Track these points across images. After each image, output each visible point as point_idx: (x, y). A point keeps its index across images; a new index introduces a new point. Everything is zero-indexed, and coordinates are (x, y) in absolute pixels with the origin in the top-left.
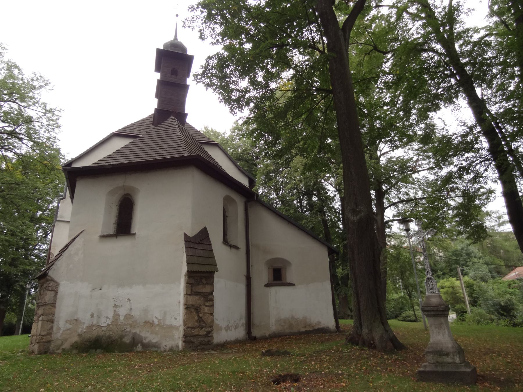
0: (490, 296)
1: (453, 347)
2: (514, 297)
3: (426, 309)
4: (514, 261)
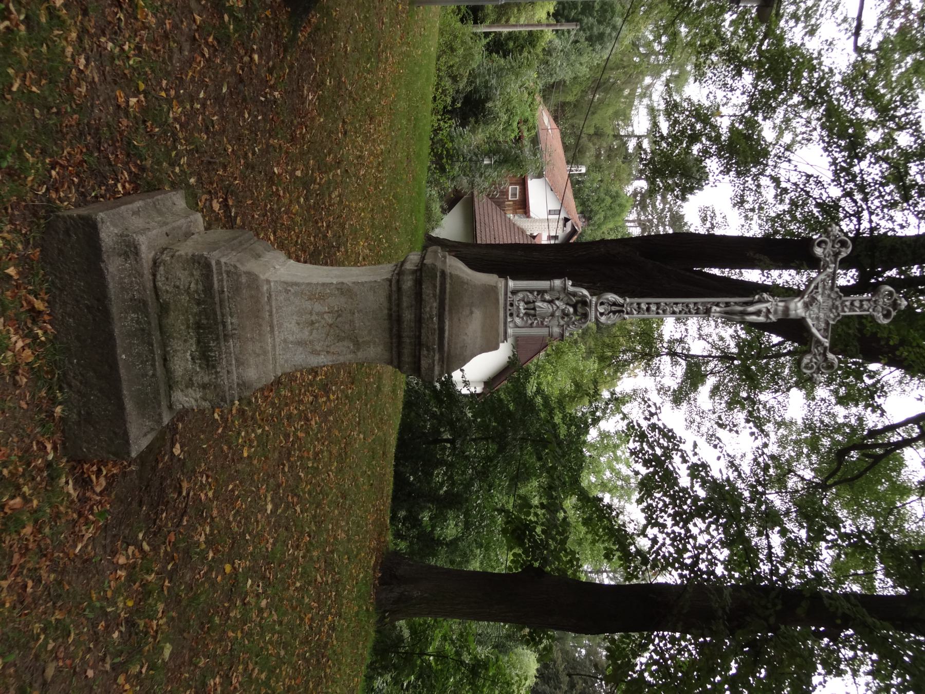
1: (243, 385)
3: (427, 290)
4: (572, 117)
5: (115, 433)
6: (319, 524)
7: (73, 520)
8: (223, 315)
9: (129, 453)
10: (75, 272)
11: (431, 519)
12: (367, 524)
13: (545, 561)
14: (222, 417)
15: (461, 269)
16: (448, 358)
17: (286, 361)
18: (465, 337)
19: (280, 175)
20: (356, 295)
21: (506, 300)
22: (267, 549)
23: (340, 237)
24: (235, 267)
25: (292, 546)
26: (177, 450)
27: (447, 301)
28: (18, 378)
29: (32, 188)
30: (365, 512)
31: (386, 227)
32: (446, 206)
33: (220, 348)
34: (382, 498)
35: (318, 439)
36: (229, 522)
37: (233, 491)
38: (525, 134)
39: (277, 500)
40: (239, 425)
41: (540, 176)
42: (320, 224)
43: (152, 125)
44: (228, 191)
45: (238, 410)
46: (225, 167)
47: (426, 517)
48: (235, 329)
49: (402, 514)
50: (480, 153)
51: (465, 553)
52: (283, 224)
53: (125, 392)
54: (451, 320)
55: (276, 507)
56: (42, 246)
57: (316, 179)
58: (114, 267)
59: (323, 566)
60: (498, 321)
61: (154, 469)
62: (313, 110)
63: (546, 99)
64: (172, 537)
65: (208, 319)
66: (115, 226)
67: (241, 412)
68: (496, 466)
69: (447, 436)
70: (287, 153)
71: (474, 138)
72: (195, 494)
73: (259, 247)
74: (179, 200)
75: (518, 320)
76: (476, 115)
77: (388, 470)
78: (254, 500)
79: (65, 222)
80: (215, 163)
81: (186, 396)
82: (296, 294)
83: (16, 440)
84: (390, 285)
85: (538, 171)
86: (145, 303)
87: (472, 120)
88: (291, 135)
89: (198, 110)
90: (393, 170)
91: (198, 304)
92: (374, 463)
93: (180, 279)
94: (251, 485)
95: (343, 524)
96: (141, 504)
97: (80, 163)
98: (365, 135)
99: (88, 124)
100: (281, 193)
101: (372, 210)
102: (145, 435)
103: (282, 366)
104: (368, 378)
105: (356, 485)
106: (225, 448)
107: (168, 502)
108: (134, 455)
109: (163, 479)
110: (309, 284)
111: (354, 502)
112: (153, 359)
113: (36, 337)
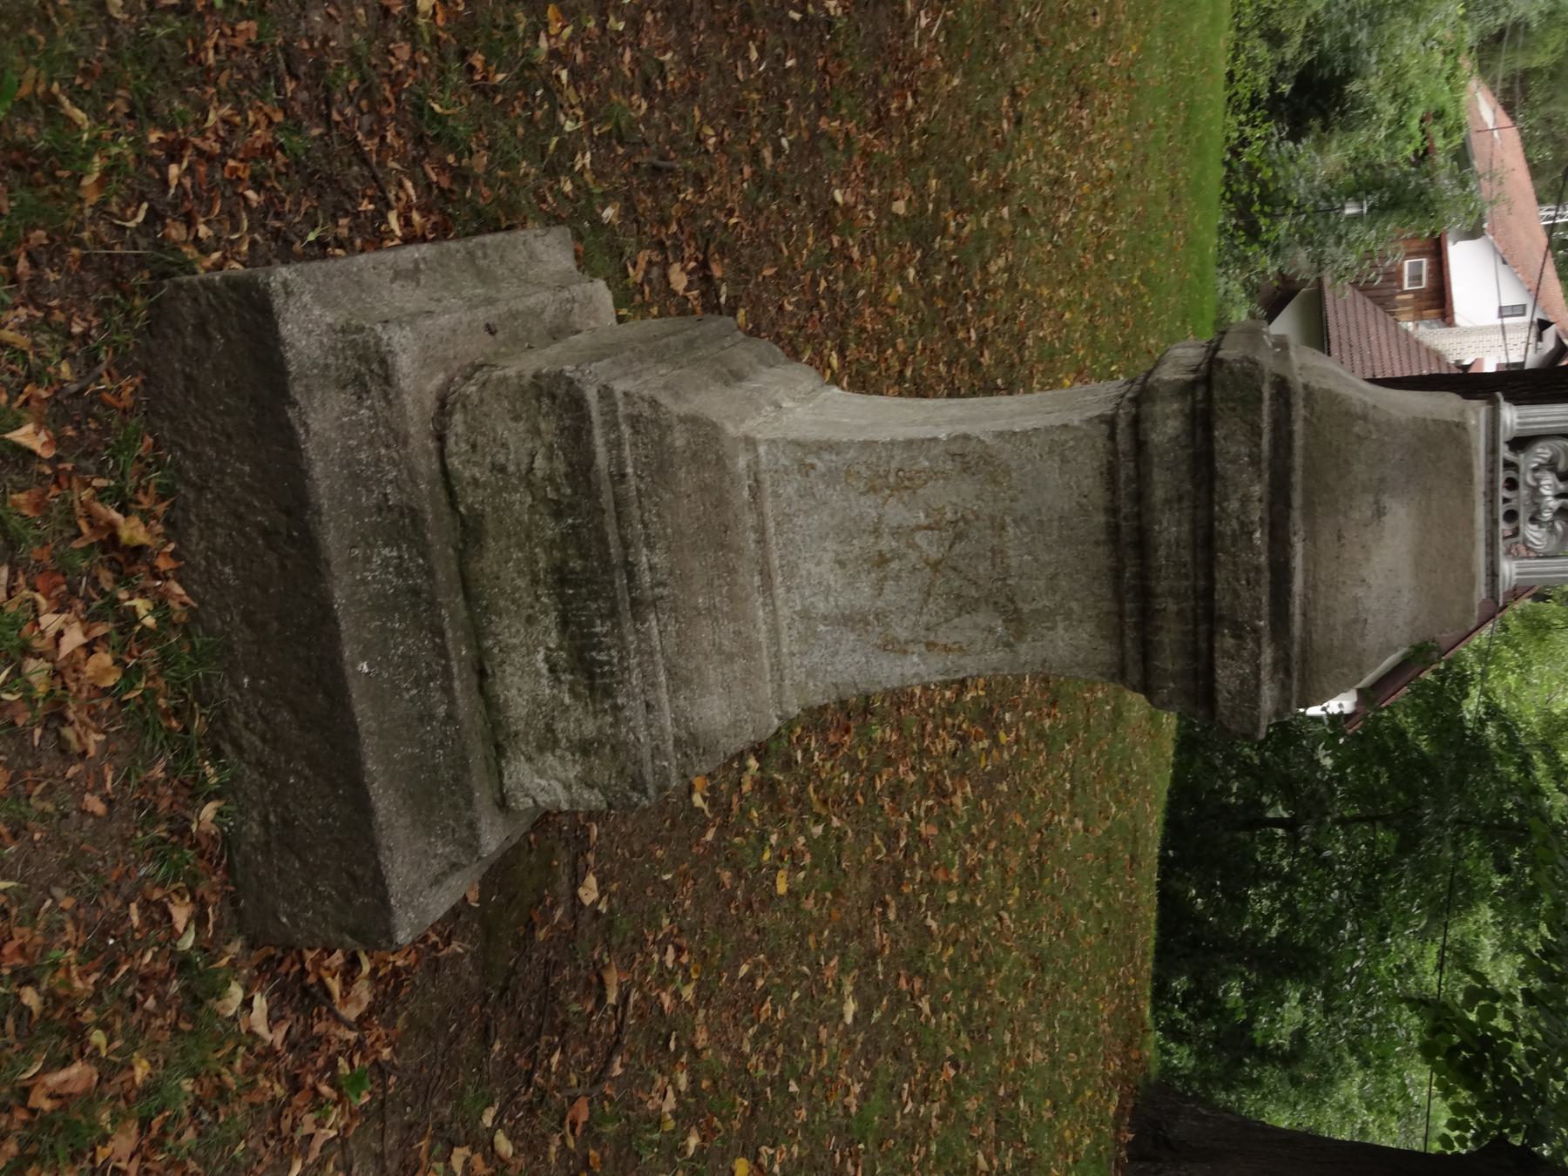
0: (1393, 36)
1: (691, 743)
2: (1383, 133)
3: (1230, 443)
4: (1546, 101)
5: (353, 878)
6: (978, 1036)
7: (273, 1101)
8: (626, 545)
9: (389, 934)
10: (229, 437)
11: (1246, 995)
12: (1096, 1023)
13: (1538, 1133)
14: (713, 801)
15: (1338, 376)
16: (1304, 660)
17: (811, 673)
18: (1360, 592)
19: (847, 209)
20: (1007, 472)
21: (1492, 471)
22: (846, 1108)
23: (1012, 366)
24: (654, 403)
25: (911, 1094)
26: (589, 892)
27: (1297, 478)
28: (68, 733)
29: (101, 206)
30: (1093, 994)
31: (1125, 347)
32: (1261, 312)
33: (622, 638)
34: (1131, 959)
35: (972, 839)
36: (739, 1055)
37: (751, 978)
38: (1439, 143)
39: (870, 991)
40: (762, 818)
41: (1474, 233)
42: (961, 335)
43: (486, 63)
44: (709, 244)
45: (759, 784)
46: (700, 183)
47: (1234, 992)
48: (663, 584)
49: (1180, 984)
50: (1331, 196)
51: (1325, 1064)
52: (863, 330)
53: (370, 765)
54: (1311, 537)
55: (866, 1007)
56: (147, 371)
57: (947, 225)
58: (323, 418)
59: (992, 1131)
60: (1471, 535)
61: (524, 943)
62: (931, 54)
63: (1484, 70)
64: (582, 1112)
65: (584, 556)
66: (330, 304)
67: (766, 787)
68: (1397, 881)
69: (1281, 812)
70: (866, 154)
71: (1322, 161)
72: (644, 997)
73: (744, 353)
74: (550, 251)
75: (1532, 533)
76: (1324, 114)
77: (1145, 896)
78: (807, 995)
79: (195, 300)
80: (671, 170)
81: (541, 773)
82: (831, 477)
83: (67, 903)
84: (1112, 437)
85: (1472, 220)
86: (415, 515)
87: (1315, 124)
88: (877, 111)
89: (620, 34)
90: (1139, 219)
91: (558, 515)
92: (1110, 882)
93: (504, 445)
94: (799, 960)
95: (1039, 1027)
96: (485, 1038)
97: (268, 151)
98: (1069, 133)
99: (287, 48)
100: (855, 253)
101: (1091, 308)
102: (437, 881)
103: (799, 687)
104: (1091, 690)
105: (1070, 937)
106: (726, 876)
107: (565, 1024)
108: (403, 936)
109: (551, 967)
110: (867, 445)
111: (1064, 975)
112: (447, 673)
113: (132, 616)
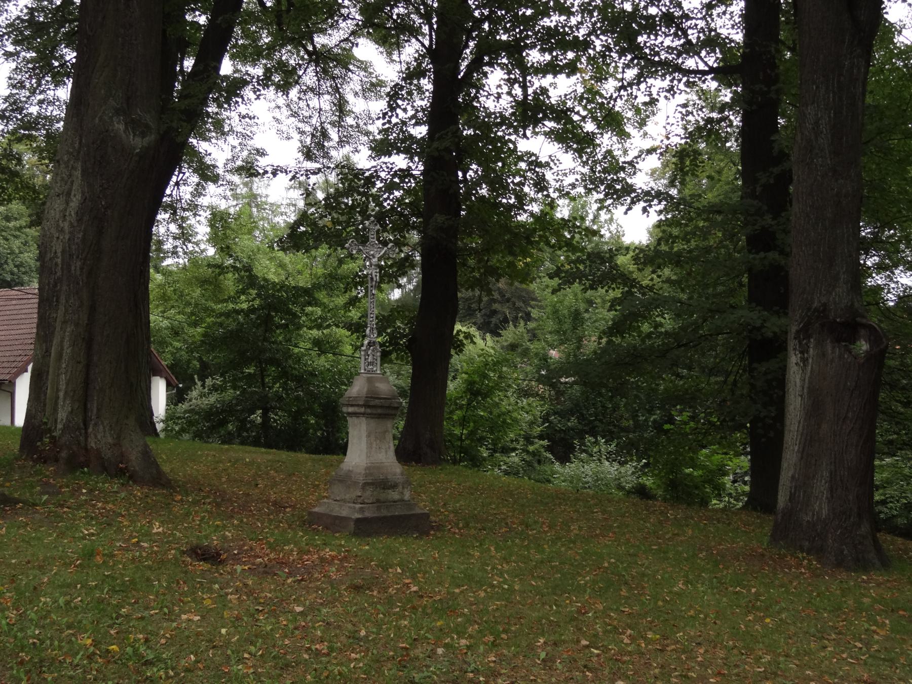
1: (402, 474)
3: (372, 403)
